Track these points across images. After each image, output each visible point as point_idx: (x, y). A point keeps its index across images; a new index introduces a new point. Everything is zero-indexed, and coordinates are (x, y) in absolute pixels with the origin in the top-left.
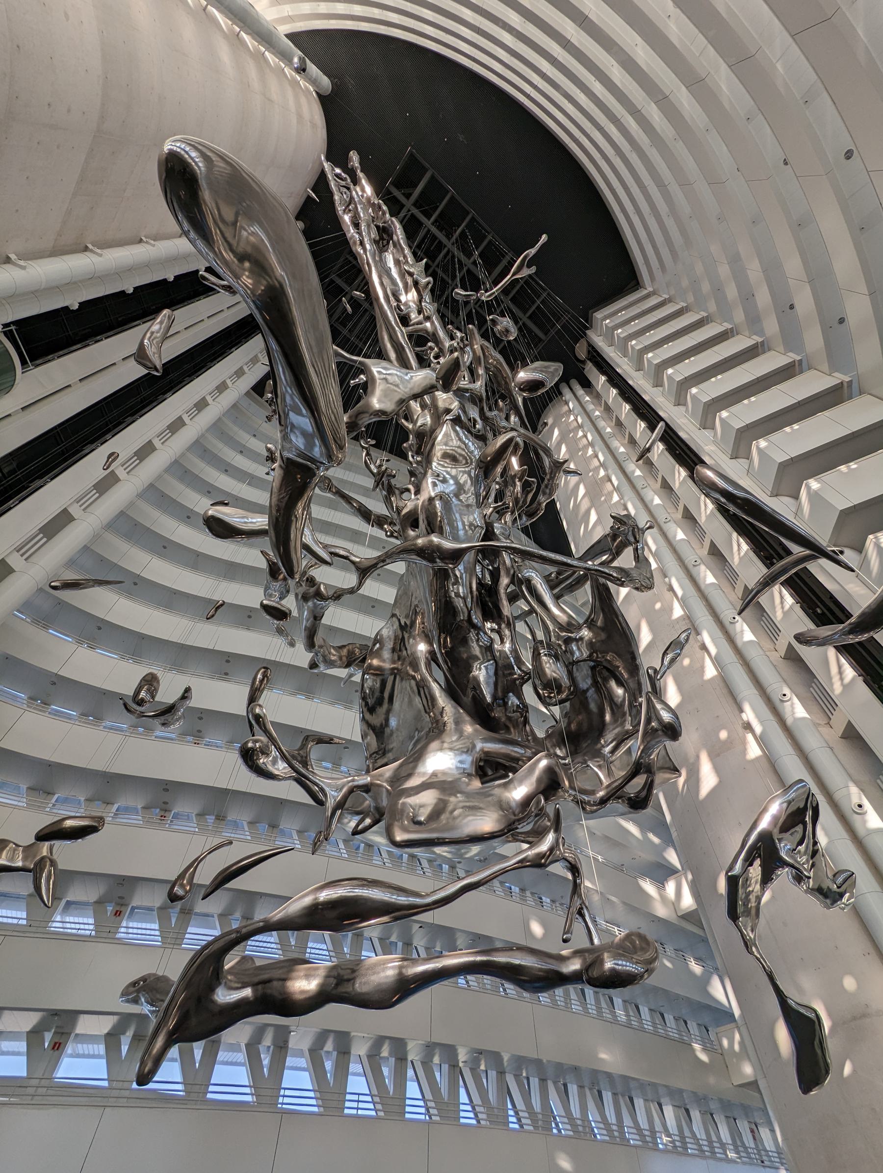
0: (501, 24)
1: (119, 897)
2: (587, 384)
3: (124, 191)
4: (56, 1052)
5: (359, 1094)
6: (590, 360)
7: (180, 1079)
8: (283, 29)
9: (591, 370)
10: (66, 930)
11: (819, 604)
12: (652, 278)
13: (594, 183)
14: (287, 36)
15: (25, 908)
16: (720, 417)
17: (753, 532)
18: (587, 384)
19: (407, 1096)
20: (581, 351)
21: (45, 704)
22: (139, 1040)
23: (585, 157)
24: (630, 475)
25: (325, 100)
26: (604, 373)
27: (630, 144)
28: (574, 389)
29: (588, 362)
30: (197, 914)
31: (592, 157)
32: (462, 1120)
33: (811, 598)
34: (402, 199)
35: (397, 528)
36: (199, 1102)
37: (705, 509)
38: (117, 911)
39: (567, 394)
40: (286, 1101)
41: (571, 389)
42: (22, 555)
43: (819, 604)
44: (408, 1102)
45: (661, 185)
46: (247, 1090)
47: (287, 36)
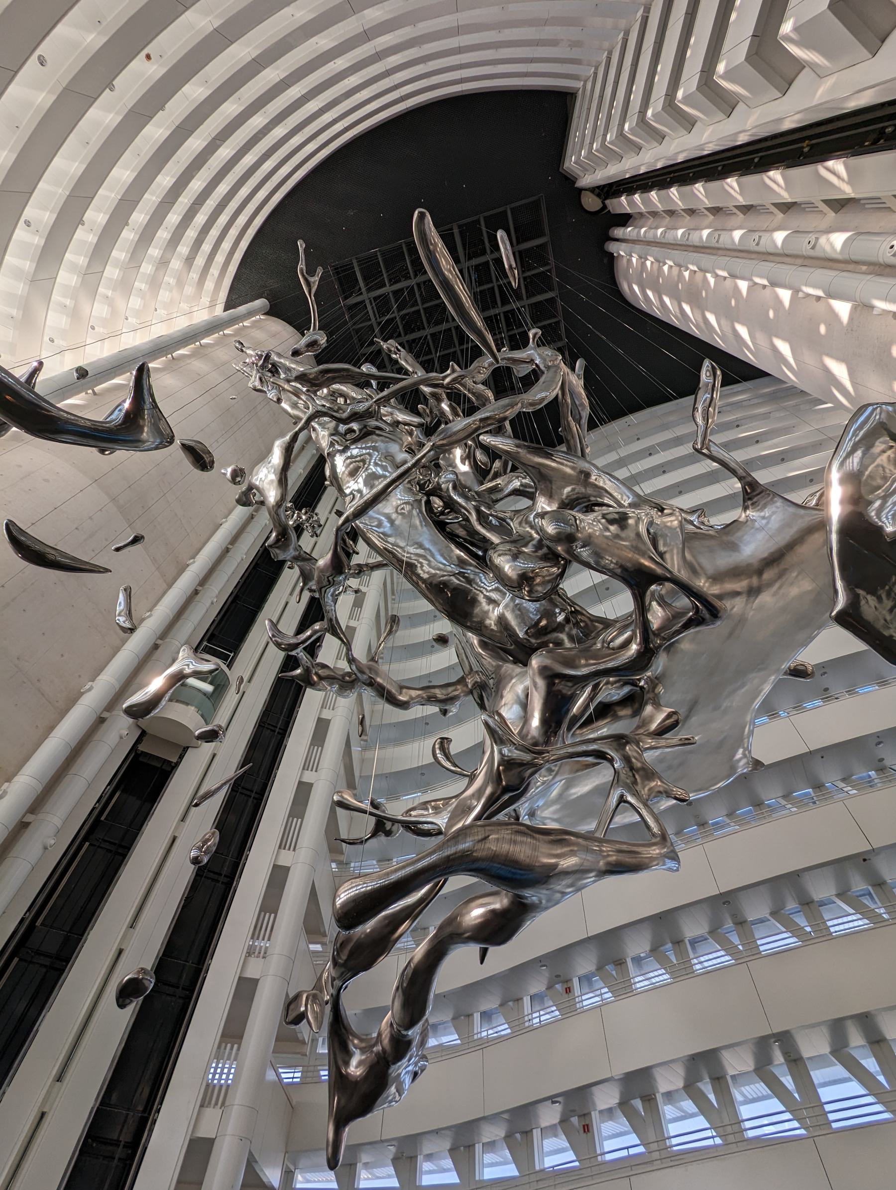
0: (261, 136)
1: (556, 976)
2: (624, 220)
3: (176, 515)
4: (589, 1134)
5: (627, 1148)
6: (606, 199)
7: (575, 1158)
8: (219, 310)
9: (623, 204)
10: (499, 1034)
11: (881, 125)
12: (575, 77)
13: (454, 95)
14: (225, 311)
15: (453, 1029)
16: (679, 101)
17: (769, 152)
18: (624, 220)
19: (823, 1100)
20: (591, 203)
21: (389, 860)
22: (649, 1100)
23: (420, 96)
24: (701, 245)
25: (273, 312)
26: (618, 194)
27: (412, 47)
28: (617, 237)
29: (607, 202)
30: (754, 923)
31: (390, 102)
32: (834, 1125)
33: (848, 136)
34: (359, 299)
35: (531, 517)
36: (594, 1177)
37: (734, 190)
38: (566, 989)
39: (612, 247)
40: (838, 1119)
41: (617, 240)
42: (312, 770)
43: (881, 125)
44: (828, 1108)
45: (458, 31)
46: (708, 1133)
47: (225, 311)
